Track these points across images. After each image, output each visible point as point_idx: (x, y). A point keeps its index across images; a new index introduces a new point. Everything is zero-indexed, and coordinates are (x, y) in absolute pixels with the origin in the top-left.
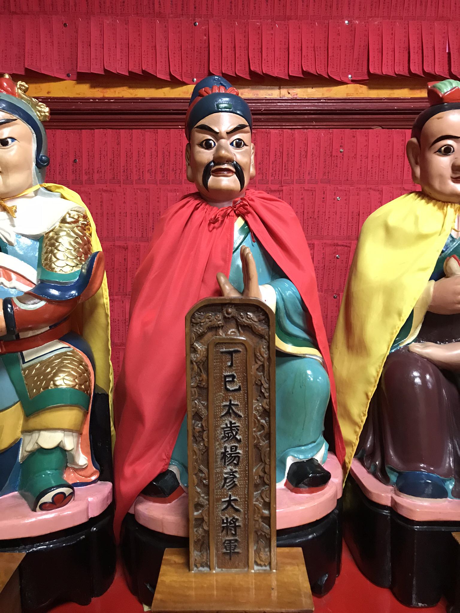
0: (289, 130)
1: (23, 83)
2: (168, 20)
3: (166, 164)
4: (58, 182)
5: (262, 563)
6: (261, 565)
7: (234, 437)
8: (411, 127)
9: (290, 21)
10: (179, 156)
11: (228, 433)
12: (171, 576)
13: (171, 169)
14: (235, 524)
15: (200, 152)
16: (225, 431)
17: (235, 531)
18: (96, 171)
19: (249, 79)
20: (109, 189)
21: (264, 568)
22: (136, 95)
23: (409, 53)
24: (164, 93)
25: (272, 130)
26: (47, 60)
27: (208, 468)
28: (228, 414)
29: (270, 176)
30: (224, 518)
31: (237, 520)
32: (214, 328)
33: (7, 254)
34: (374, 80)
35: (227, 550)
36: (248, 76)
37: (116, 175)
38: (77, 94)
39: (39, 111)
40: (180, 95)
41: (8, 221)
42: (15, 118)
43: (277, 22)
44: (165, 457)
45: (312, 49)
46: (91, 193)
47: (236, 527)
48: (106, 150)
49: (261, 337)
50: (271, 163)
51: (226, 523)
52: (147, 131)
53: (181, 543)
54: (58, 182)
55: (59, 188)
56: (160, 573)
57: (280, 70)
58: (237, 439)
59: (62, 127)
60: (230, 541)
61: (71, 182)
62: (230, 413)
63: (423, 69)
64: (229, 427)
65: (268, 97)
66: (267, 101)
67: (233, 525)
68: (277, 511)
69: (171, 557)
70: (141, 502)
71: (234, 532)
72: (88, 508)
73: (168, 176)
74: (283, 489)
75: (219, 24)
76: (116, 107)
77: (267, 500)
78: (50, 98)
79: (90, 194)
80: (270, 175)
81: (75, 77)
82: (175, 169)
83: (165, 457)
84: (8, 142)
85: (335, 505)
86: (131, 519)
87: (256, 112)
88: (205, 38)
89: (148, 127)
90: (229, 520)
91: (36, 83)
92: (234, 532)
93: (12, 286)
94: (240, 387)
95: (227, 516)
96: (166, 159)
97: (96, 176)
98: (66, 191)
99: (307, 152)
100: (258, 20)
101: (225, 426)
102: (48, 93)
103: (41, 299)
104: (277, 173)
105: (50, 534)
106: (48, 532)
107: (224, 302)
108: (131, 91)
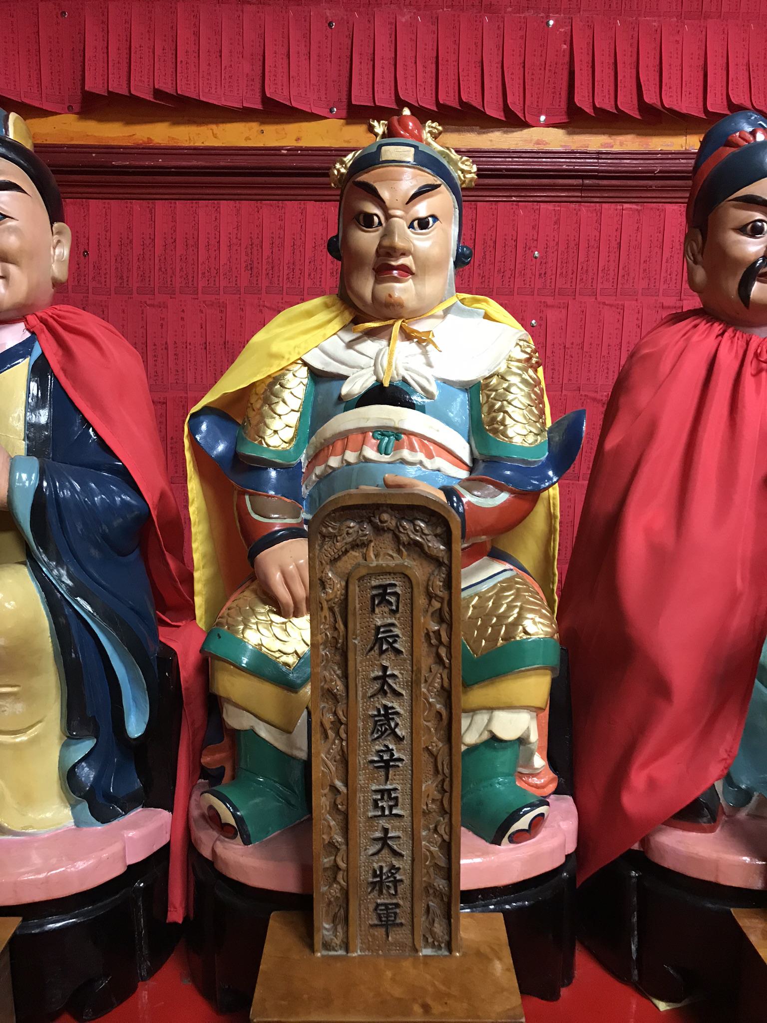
1: (435, 124)
2: (503, 17)
3: (487, 261)
4: (474, 291)
8: (687, 200)
9: (709, 21)
11: (381, 726)
13: (496, 270)
14: (395, 878)
15: (739, 242)
16: (376, 722)
17: (396, 891)
19: (260, 107)
23: (572, 74)
25: (668, 206)
26: (299, 85)
27: (346, 785)
28: (382, 692)
29: (662, 283)
30: (376, 866)
33: (424, 412)
35: (381, 921)
36: (502, 114)
38: (345, 141)
39: (463, 171)
41: (422, 357)
42: (439, 182)
43: (686, 21)
44: (725, 756)
45: (745, 68)
47: (396, 882)
48: (556, 240)
50: (307, 261)
53: (299, 905)
54: (474, 291)
55: (478, 301)
56: (677, 109)
57: (691, 103)
59: (190, 197)
60: (385, 905)
61: (640, 291)
62: (385, 693)
65: (666, 148)
66: (664, 156)
68: (462, 862)
69: (278, 935)
70: (660, 830)
71: (393, 892)
72: (124, 848)
73: (491, 280)
74: (71, 829)
75: (590, 23)
78: (301, 149)
80: (662, 280)
81: (344, 113)
83: (725, 756)
84: (428, 222)
86: (642, 860)
88: (565, 46)
91: (277, 123)
93: (435, 467)
95: (384, 861)
96: (488, 253)
98: (493, 307)
100: (656, 18)
102: (298, 139)
103: (502, 489)
104: (674, 277)
105: (524, 881)
106: (522, 879)
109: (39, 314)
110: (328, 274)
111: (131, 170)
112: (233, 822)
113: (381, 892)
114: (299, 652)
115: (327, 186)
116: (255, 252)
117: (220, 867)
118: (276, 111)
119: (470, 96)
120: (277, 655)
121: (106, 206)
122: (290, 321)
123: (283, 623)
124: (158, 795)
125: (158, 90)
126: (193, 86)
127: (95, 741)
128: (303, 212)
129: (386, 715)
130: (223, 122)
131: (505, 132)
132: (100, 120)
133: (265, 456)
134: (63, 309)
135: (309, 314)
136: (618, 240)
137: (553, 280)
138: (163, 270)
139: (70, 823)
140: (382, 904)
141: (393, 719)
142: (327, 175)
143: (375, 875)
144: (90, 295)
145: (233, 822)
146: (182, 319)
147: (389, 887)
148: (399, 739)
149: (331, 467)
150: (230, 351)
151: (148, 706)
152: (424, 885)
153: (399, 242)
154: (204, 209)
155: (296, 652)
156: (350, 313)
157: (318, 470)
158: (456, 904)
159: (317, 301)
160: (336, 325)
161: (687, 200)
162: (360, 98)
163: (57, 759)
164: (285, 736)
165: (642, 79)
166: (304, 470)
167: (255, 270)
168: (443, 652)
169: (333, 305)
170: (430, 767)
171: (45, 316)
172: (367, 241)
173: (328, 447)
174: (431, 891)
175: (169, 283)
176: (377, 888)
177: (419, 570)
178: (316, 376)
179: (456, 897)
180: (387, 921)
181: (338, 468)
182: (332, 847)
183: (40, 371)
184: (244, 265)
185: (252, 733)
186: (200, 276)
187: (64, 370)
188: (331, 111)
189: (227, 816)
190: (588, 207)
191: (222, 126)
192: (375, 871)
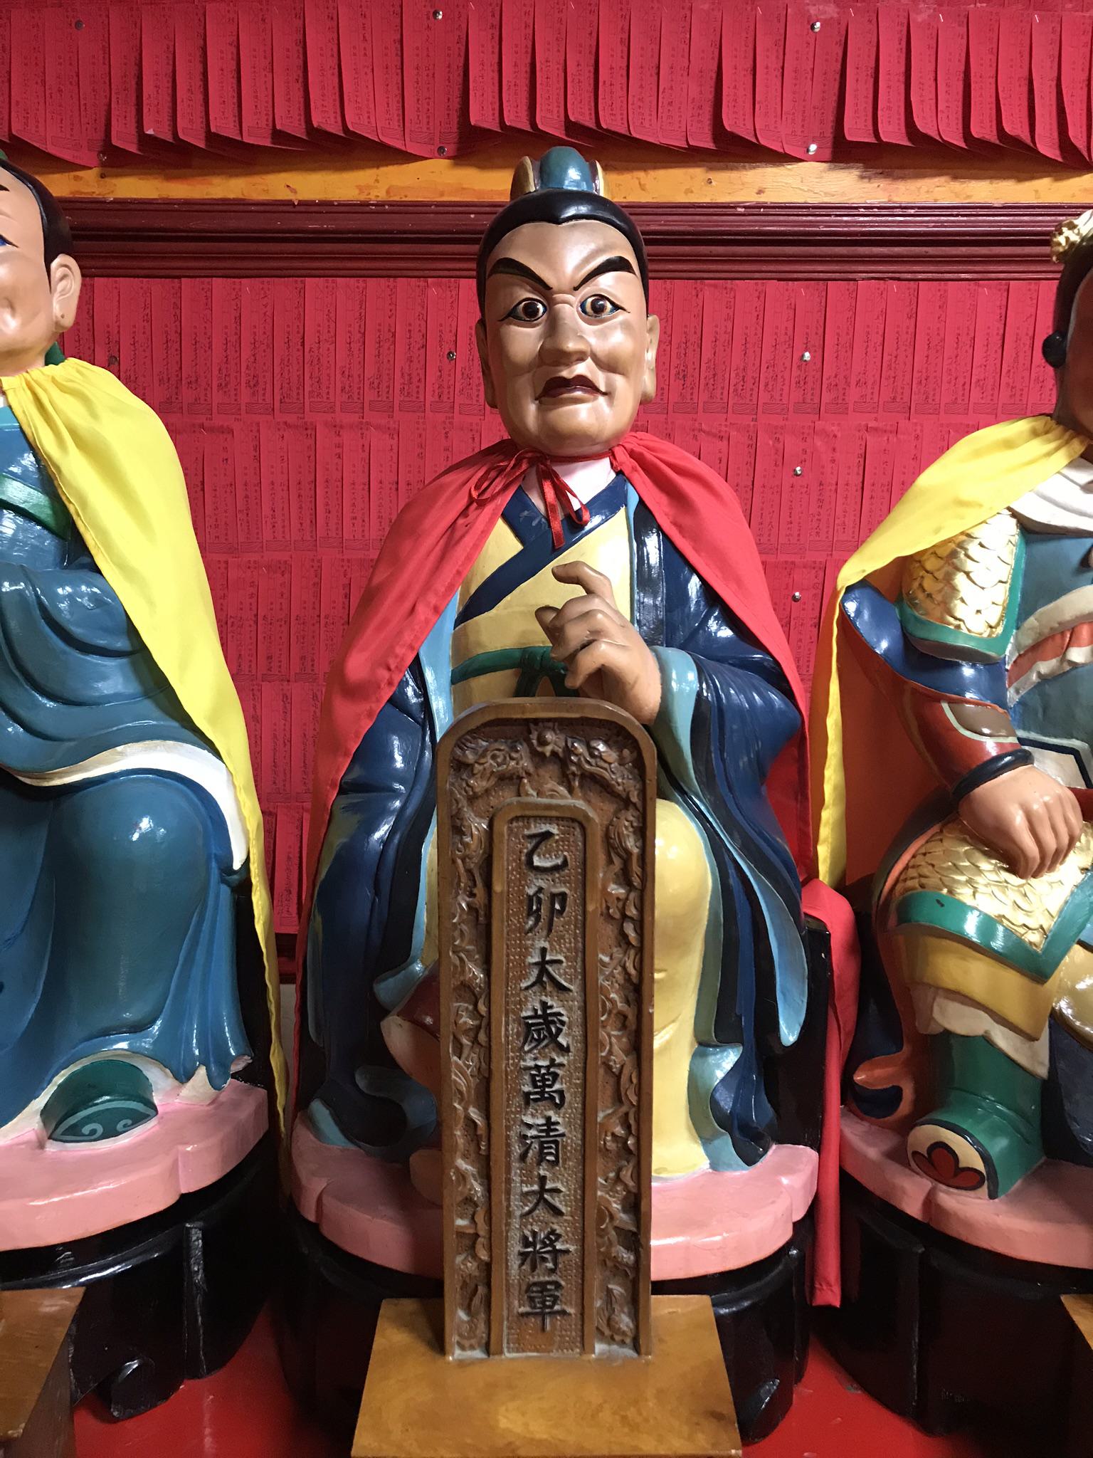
0: (353, 280)
7: (553, 1038)
8: (1058, 276)
10: (387, 345)
12: (400, 1390)
17: (556, 1264)
18: (853, 383)
19: (711, 146)
20: (881, 425)
22: (968, 197)
24: (1037, 191)
31: (558, 1236)
32: (511, 780)
36: (1058, 152)
37: (900, 390)
40: (1073, 196)
46: (839, 435)
47: (556, 1253)
49: (626, 803)
51: (533, 1244)
52: (983, 286)
58: (560, 1046)
63: (566, 116)
68: (654, 1243)
69: (392, 1337)
71: (550, 1265)
79: (835, 436)
81: (828, 153)
82: (133, 378)
85: (787, 1234)
87: (656, 239)
89: (711, 275)
92: (550, 1265)
94: (565, 862)
96: (1021, 355)
97: (854, 394)
99: (425, 336)
101: (530, 1013)
108: (957, 186)
109: (628, 446)
110: (793, 384)
112: (979, 1165)
113: (534, 1268)
114: (1045, 927)
115: (1045, 259)
116: (690, 351)
117: (327, 1231)
118: (734, 150)
119: (1015, 126)
120: (1022, 930)
122: (978, 453)
123: (1022, 886)
124: (802, 1126)
125: (575, 124)
126: (619, 117)
127: (741, 1049)
128: (762, 296)
129: (545, 1016)
130: (655, 168)
131: (1057, 179)
132: (482, 167)
133: (961, 643)
134: (649, 438)
135: (1009, 444)
136: (1031, 333)
137: (755, 393)
139: (703, 1163)
140: (535, 1284)
141: (553, 1022)
142: (1047, 243)
143: (526, 1243)
145: (979, 1165)
147: (544, 1260)
148: (564, 1050)
149: (1071, 663)
150: (882, 493)
151: (805, 1000)
152: (601, 1258)
153: (571, 345)
155: (1042, 927)
156: (1082, 442)
157: (1045, 667)
159: (1022, 426)
160: (1061, 458)
161: (1058, 276)
162: (856, 130)
163: (686, 1074)
164: (1028, 1044)
165: (914, 99)
166: (1008, 667)
167: (689, 380)
168: (630, 930)
169: (1047, 432)
170: (609, 1091)
171: (638, 449)
172: (524, 340)
173: (1063, 634)
174: (609, 1264)
176: (528, 1261)
177: (595, 811)
178: (1031, 531)
181: (1083, 665)
183: (643, 522)
184: (673, 372)
185: (986, 1040)
186: (702, 387)
187: (675, 524)
188: (441, 150)
189: (969, 1156)
190: (716, 286)
191: (653, 174)
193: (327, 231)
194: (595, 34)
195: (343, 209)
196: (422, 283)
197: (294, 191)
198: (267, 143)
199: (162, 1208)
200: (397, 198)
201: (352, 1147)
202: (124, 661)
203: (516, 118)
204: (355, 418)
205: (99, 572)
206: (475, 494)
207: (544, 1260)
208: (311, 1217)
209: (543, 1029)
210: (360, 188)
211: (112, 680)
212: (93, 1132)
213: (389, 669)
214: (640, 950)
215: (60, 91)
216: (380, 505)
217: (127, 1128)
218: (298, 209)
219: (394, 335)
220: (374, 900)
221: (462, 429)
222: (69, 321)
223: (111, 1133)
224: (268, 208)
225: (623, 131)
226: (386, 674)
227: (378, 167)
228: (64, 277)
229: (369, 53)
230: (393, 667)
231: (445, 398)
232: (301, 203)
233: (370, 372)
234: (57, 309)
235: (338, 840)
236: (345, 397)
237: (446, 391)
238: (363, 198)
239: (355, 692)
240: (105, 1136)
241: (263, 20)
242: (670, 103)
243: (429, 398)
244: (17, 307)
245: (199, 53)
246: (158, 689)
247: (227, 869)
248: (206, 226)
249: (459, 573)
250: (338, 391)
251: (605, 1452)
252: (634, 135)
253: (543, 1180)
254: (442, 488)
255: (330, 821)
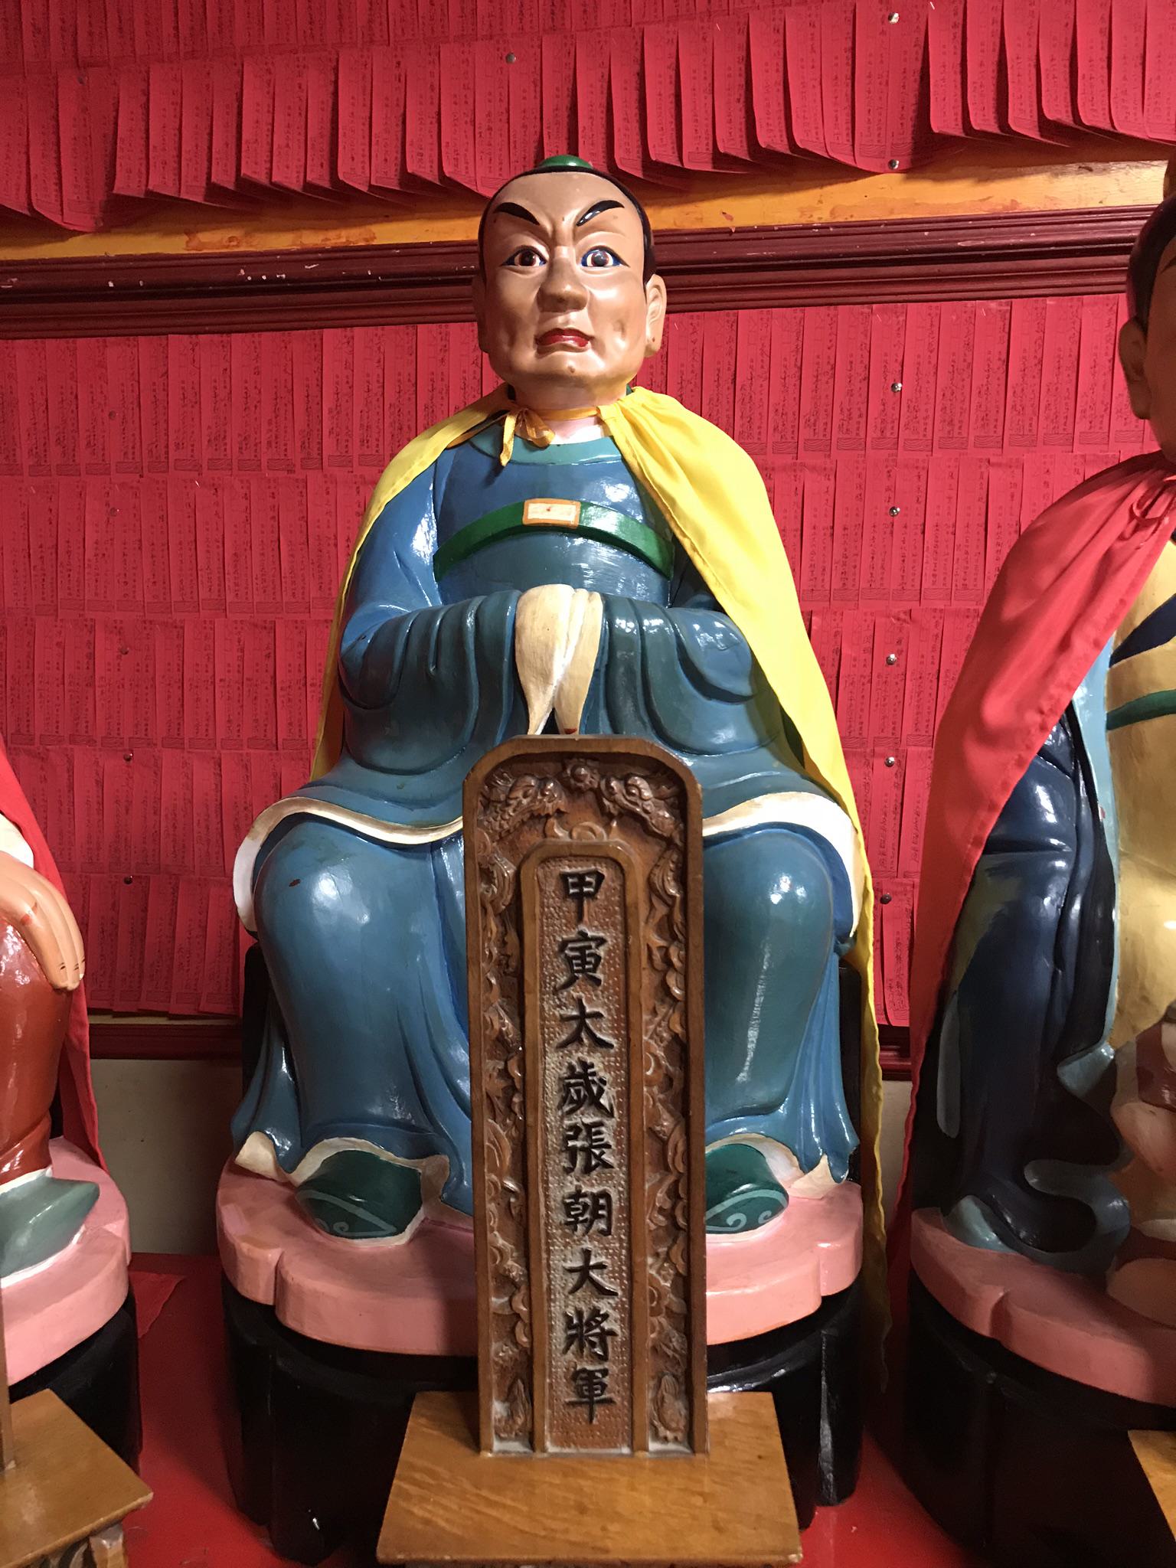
5: (669, 1434)
6: (665, 1440)
12: (433, 1492)
16: (570, 1085)
19: (639, 175)
21: (671, 1446)
30: (571, 1312)
31: (606, 1317)
32: (538, 818)
34: (929, 154)
49: (669, 842)
53: (453, 1376)
58: (601, 1107)
62: (581, 1041)
63: (209, 178)
64: (579, 1076)
67: (597, 1330)
68: (708, 1294)
76: (676, 257)
77: (678, 1029)
90: (586, 1316)
95: (582, 1302)
107: (569, 748)
111: (983, 253)
121: (695, 321)
128: (350, 341)
129: (584, 1075)
138: (1019, 408)
144: (869, 451)
146: (1046, 484)
147: (593, 1345)
154: (880, 317)
158: (700, 1373)
175: (1027, 427)
179: (701, 1361)
180: (591, 1397)
182: (505, 1282)
188: (891, 164)
192: (569, 1319)
193: (768, 259)
194: (1071, 26)
195: (782, 234)
196: (865, 309)
197: (731, 218)
198: (708, 168)
199: (812, 1311)
200: (841, 219)
201: (1012, 1253)
202: (740, 708)
203: (984, 120)
204: (789, 459)
205: (718, 608)
206: (1137, 513)
207: (593, 1345)
208: (984, 1329)
209: (581, 1089)
210: (802, 212)
211: (729, 729)
212: (737, 1222)
213: (1042, 712)
214: (688, 1231)
215: (490, 129)
216: (813, 553)
217: (767, 1219)
218: (735, 236)
219: (834, 368)
220: (1055, 973)
221: (906, 466)
222: (657, 346)
223: (752, 1225)
224: (706, 237)
225: (1107, 127)
226: (1038, 718)
227: (822, 186)
228: (656, 297)
229: (817, 64)
230: (1046, 709)
231: (888, 434)
232: (739, 230)
233: (806, 407)
234: (648, 333)
235: (989, 907)
236: (778, 437)
237: (889, 426)
238: (804, 220)
239: (990, 738)
240: (746, 1229)
241: (704, 39)
242: (1157, 95)
243: (872, 434)
244: (628, 330)
245: (635, 79)
246: (784, 739)
247: (843, 937)
248: (692, 257)
249: (1122, 602)
250: (771, 430)
251: (666, 1556)
252: (1121, 131)
253: (587, 1254)
254: (1081, 515)
255: (972, 883)
